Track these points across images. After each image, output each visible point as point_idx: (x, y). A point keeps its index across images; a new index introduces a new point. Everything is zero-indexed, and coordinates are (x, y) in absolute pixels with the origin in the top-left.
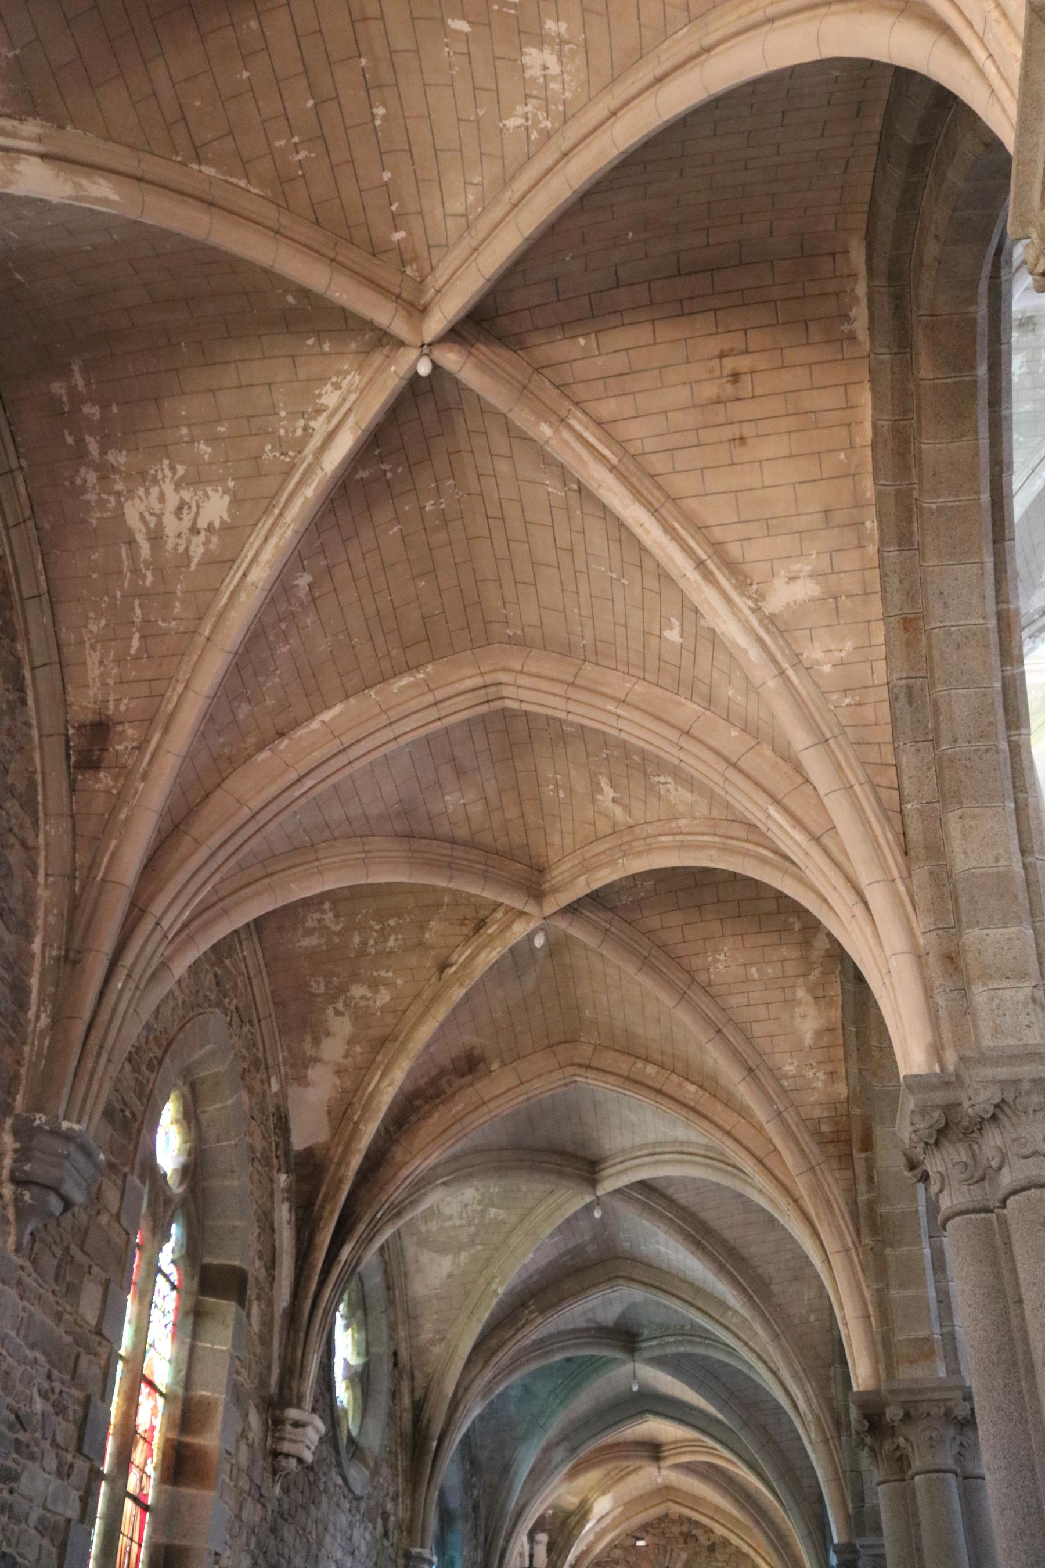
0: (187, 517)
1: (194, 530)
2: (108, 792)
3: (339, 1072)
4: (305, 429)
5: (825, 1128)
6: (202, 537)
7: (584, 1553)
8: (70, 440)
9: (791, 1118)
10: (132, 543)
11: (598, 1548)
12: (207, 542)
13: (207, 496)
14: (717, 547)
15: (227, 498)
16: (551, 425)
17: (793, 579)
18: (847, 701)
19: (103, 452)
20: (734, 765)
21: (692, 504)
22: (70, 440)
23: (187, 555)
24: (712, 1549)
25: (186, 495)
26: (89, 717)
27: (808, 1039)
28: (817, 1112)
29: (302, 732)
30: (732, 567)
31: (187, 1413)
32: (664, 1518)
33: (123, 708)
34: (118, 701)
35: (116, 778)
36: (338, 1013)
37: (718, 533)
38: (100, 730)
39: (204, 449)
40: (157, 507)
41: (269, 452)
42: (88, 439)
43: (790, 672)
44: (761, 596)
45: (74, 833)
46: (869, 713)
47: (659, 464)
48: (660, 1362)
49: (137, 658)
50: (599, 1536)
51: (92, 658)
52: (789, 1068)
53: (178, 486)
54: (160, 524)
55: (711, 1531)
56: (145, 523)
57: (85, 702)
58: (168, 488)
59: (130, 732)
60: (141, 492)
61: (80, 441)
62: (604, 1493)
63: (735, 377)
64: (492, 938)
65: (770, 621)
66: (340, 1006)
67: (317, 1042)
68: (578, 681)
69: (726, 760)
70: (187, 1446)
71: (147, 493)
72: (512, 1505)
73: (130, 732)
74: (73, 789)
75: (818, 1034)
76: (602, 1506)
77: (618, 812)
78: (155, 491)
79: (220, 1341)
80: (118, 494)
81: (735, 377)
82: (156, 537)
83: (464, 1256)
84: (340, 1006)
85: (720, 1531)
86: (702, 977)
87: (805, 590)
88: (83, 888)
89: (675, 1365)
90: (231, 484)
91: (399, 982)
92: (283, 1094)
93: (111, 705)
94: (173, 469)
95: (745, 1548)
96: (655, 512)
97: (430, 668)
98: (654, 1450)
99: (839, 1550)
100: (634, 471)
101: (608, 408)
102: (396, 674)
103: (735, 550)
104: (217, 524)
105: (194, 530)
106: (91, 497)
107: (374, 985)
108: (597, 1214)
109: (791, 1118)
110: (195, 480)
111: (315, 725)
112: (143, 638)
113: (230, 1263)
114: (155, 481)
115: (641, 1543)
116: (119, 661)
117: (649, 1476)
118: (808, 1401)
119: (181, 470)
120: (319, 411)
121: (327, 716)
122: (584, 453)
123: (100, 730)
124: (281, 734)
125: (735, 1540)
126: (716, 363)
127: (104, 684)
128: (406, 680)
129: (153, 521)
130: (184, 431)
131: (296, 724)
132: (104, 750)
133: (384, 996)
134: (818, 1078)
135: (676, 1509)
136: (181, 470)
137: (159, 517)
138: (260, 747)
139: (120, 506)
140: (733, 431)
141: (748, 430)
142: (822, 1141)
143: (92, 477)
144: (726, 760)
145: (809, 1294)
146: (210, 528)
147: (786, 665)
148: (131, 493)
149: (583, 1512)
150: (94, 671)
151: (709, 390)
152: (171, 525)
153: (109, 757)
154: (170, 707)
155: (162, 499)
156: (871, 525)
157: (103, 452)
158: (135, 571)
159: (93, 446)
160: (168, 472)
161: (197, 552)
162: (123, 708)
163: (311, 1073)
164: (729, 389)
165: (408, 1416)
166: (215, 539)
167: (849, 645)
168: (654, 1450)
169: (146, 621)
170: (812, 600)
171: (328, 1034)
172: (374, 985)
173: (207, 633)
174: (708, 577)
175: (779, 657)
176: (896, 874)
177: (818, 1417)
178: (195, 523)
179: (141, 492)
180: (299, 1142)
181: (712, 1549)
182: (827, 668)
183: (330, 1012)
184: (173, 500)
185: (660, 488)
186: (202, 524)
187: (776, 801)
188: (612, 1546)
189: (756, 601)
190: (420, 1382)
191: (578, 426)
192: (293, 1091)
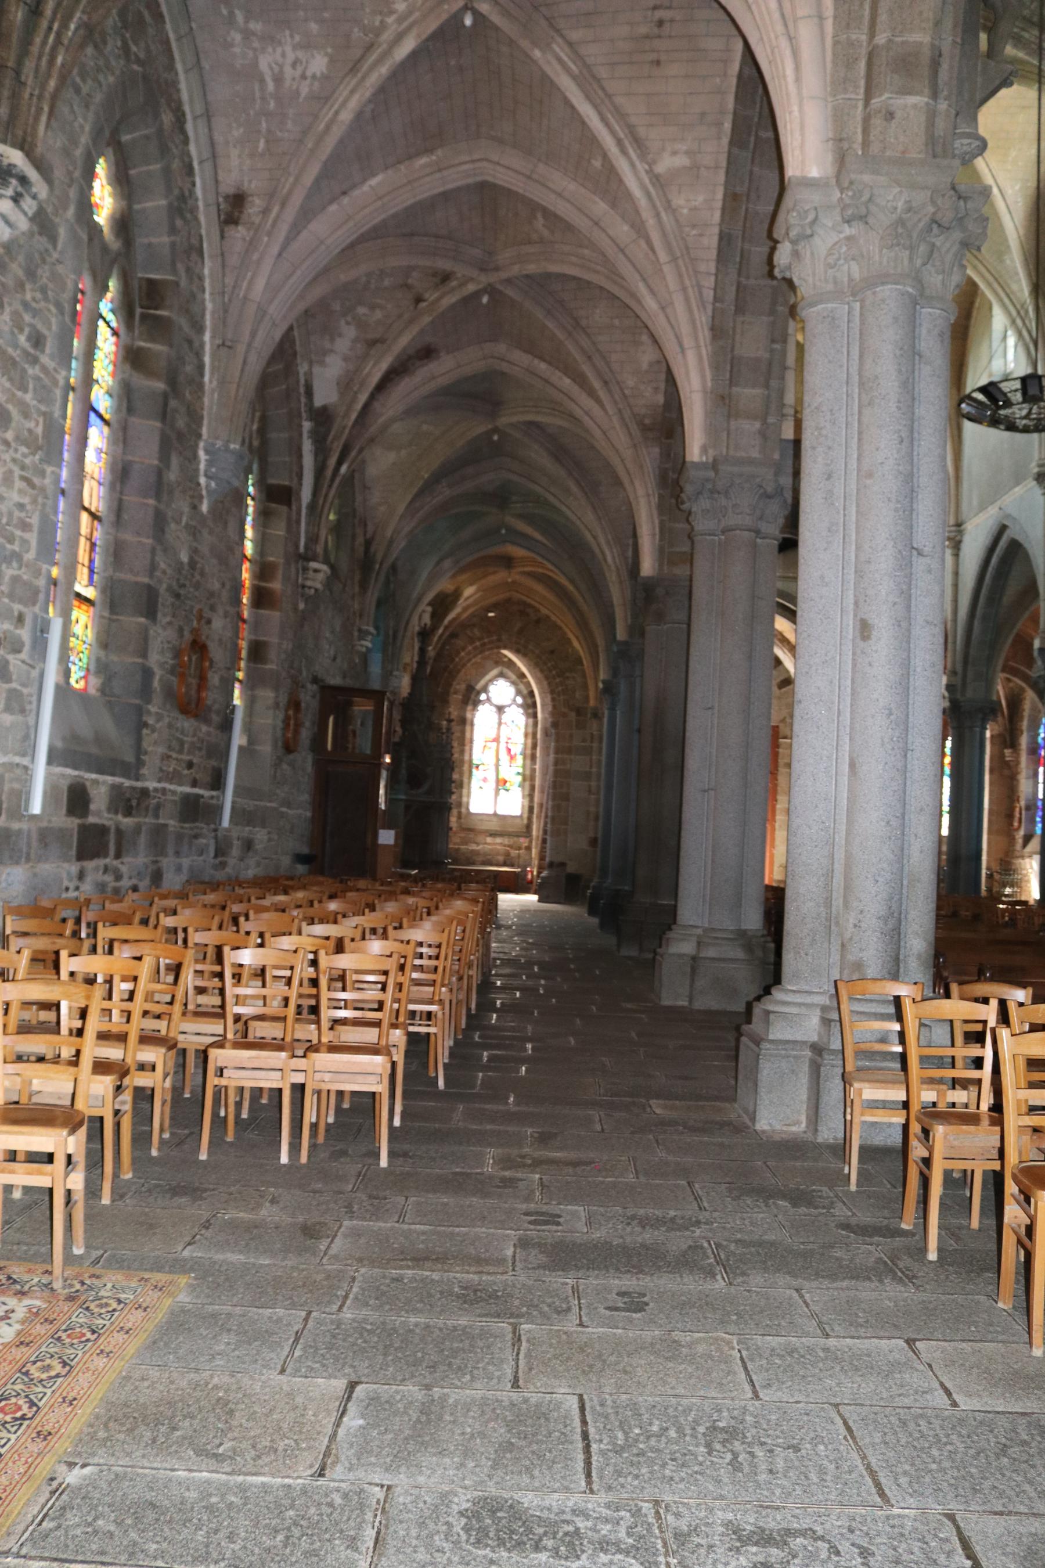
0: (299, 69)
1: (304, 77)
2: (244, 239)
3: (346, 359)
4: (382, 22)
5: (647, 421)
6: (308, 82)
7: (454, 619)
8: (225, 12)
9: (627, 414)
10: (262, 81)
11: (465, 615)
12: (312, 85)
13: (313, 56)
14: (631, 130)
15: (326, 60)
16: (541, 50)
17: (674, 153)
18: (694, 232)
19: (246, 22)
20: (622, 251)
21: (619, 100)
22: (225, 12)
23: (298, 92)
24: (538, 621)
25: (300, 54)
26: (231, 191)
27: (645, 366)
28: (643, 411)
29: (356, 193)
30: (638, 143)
31: (264, 571)
32: (508, 600)
33: (253, 186)
34: (250, 181)
35: (249, 229)
36: (348, 323)
37: (633, 120)
38: (238, 200)
39: (314, 27)
40: (280, 60)
41: (356, 33)
42: (237, 12)
43: (663, 214)
44: (654, 162)
45: (223, 266)
46: (705, 241)
47: (603, 72)
48: (521, 516)
49: (262, 155)
50: (465, 609)
51: (234, 153)
52: (631, 383)
53: (295, 47)
54: (281, 71)
55: (539, 611)
56: (271, 69)
57: (229, 183)
58: (288, 49)
59: (257, 201)
60: (270, 50)
61: (231, 14)
62: (471, 585)
63: (660, 23)
64: (453, 289)
65: (656, 179)
66: (349, 319)
67: (332, 340)
68: (535, 176)
69: (618, 246)
70: (264, 588)
71: (274, 51)
72: (415, 595)
73: (257, 201)
74: (222, 237)
75: (651, 364)
76: (469, 591)
77: (546, 233)
78: (279, 50)
79: (279, 531)
80: (255, 50)
81: (660, 23)
82: (278, 80)
83: (403, 453)
84: (349, 319)
85: (544, 611)
86: (584, 323)
87: (681, 161)
88: (230, 300)
89: (529, 519)
90: (329, 50)
91: (389, 306)
92: (309, 375)
93: (246, 184)
94: (292, 36)
95: (559, 622)
96: (595, 106)
97: (439, 152)
98: (508, 562)
99: (604, 682)
100: (589, 80)
101: (575, 35)
102: (418, 154)
103: (642, 132)
104: (318, 74)
105: (304, 77)
106: (237, 50)
107: (373, 307)
108: (496, 438)
109: (627, 414)
110: (308, 45)
111: (365, 188)
112: (267, 142)
113: (281, 482)
114: (280, 43)
115: (491, 614)
116: (252, 155)
117: (501, 575)
118: (614, 558)
119: (297, 38)
120: (392, 12)
121: (373, 182)
122: (558, 67)
123: (238, 200)
124: (344, 193)
125: (553, 618)
126: (650, 13)
127: (241, 170)
128: (423, 160)
129: (276, 69)
130: (301, 13)
131: (354, 186)
132: (241, 212)
133: (378, 314)
134: (648, 392)
135: (517, 596)
136: (297, 38)
137: (281, 67)
138: (331, 202)
139: (256, 58)
140: (653, 56)
141: (663, 57)
142: (645, 429)
143: (238, 37)
144: (618, 246)
145: (647, 356)
146: (314, 77)
147: (661, 209)
148: (263, 50)
149: (456, 595)
150: (235, 162)
151: (643, 30)
152: (288, 71)
153: (244, 217)
154: (285, 191)
155: (283, 55)
156: (728, 126)
157: (246, 22)
158: (263, 99)
159: (240, 17)
160: (288, 39)
161: (304, 91)
162: (253, 186)
163: (328, 360)
164: (656, 30)
165: (362, 549)
166: (316, 84)
167: (701, 198)
168: (508, 562)
169: (269, 131)
170: (684, 167)
171: (340, 335)
172: (373, 307)
173: (310, 146)
174: (624, 151)
175: (658, 204)
176: (702, 343)
177: (618, 569)
178: (304, 73)
179: (270, 50)
180: (318, 402)
181: (538, 621)
182: (685, 211)
183: (343, 322)
184: (291, 56)
185: (603, 89)
186: (309, 74)
187: (644, 280)
188: (473, 615)
189: (650, 165)
190: (370, 528)
191: (558, 50)
192: (316, 370)
